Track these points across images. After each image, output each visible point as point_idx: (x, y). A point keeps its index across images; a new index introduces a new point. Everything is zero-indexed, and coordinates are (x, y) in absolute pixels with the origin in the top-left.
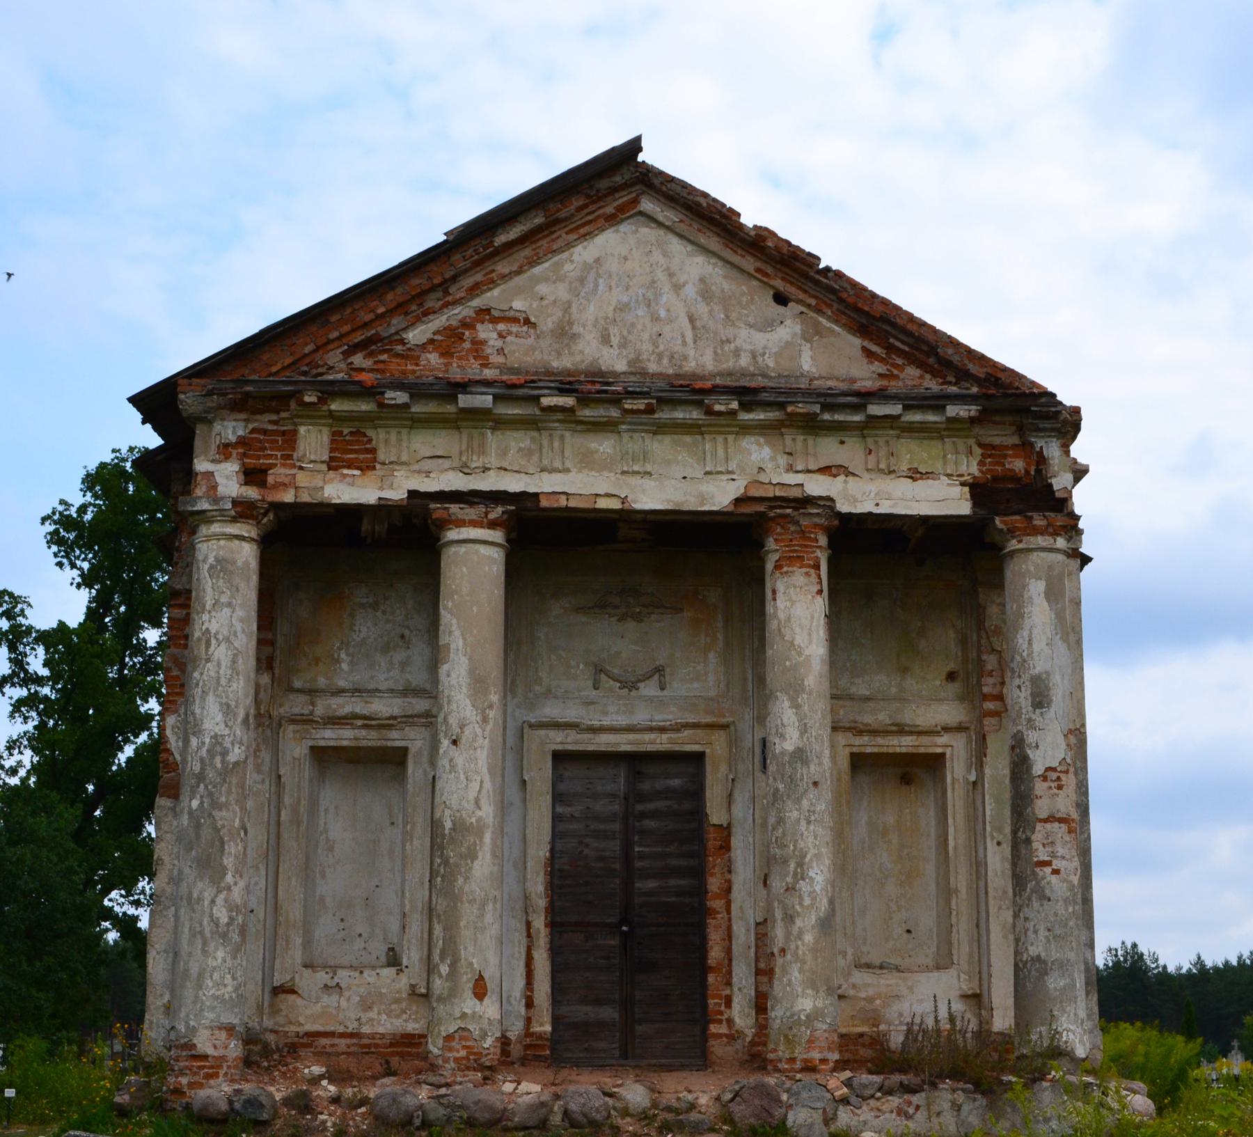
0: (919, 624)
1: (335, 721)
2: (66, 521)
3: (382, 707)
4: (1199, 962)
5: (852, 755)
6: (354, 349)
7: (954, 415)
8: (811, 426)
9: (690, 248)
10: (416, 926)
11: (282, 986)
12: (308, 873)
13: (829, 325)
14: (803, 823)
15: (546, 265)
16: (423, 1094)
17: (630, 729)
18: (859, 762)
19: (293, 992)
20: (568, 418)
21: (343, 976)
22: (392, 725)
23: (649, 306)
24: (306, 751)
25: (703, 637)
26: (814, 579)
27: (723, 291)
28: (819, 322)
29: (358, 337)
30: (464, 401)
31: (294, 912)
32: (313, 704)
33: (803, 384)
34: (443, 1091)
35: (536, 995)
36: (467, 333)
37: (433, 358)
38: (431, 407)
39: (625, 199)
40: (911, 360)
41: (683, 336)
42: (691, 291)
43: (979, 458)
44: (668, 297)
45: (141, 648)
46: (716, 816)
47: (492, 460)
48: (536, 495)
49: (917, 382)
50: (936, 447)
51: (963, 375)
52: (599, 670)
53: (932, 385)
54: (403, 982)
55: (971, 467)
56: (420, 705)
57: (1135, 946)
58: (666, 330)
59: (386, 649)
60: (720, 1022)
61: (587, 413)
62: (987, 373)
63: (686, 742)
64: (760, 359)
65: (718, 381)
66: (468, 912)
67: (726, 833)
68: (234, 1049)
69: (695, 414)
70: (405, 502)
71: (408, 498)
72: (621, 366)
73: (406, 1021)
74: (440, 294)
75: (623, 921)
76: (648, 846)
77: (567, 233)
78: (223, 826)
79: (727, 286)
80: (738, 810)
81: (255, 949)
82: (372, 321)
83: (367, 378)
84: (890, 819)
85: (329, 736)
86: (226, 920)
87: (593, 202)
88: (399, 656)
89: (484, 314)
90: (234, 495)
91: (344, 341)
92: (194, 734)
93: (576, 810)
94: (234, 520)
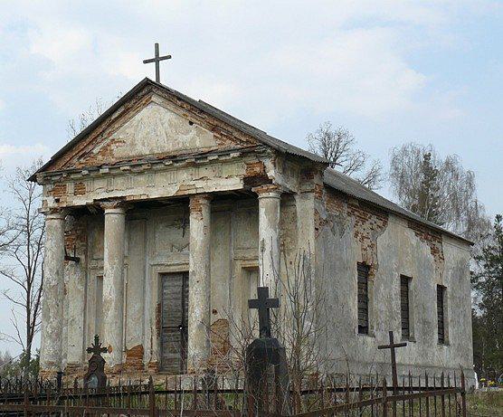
17: (178, 265)
29: (81, 154)
30: (102, 171)
37: (100, 157)
42: (166, 125)
55: (243, 172)
61: (222, 159)
72: (148, 153)
94: (51, 214)
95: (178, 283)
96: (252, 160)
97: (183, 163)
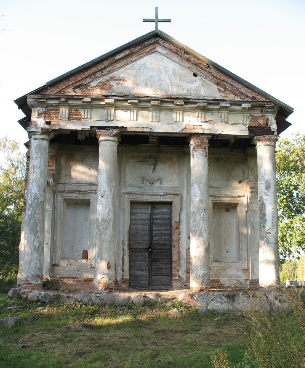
0: (232, 168)
1: (71, 192)
5: (213, 203)
7: (244, 107)
9: (170, 61)
11: (55, 264)
13: (209, 82)
14: (201, 221)
15: (130, 65)
19: (58, 266)
20: (135, 106)
22: (86, 193)
23: (159, 76)
24: (62, 200)
25: (172, 170)
26: (204, 152)
27: (179, 73)
28: (206, 82)
29: (77, 84)
32: (65, 187)
33: (202, 98)
34: (98, 295)
35: (125, 268)
36: (108, 83)
39: (152, 47)
41: (168, 84)
42: (170, 73)
43: (251, 119)
48: (126, 128)
49: (233, 98)
52: (143, 179)
58: (163, 83)
60: (176, 276)
62: (253, 96)
63: (168, 199)
64: (190, 91)
65: (178, 97)
67: (178, 224)
70: (89, 129)
71: (91, 128)
73: (89, 274)
74: (100, 72)
75: (150, 248)
76: (156, 227)
77: (136, 56)
78: (37, 219)
82: (81, 80)
85: (68, 196)
86: (38, 246)
87: (143, 48)
89: (112, 78)
90: (42, 127)
91: (74, 85)
92: (30, 193)
95: (146, 211)
97: (194, 106)
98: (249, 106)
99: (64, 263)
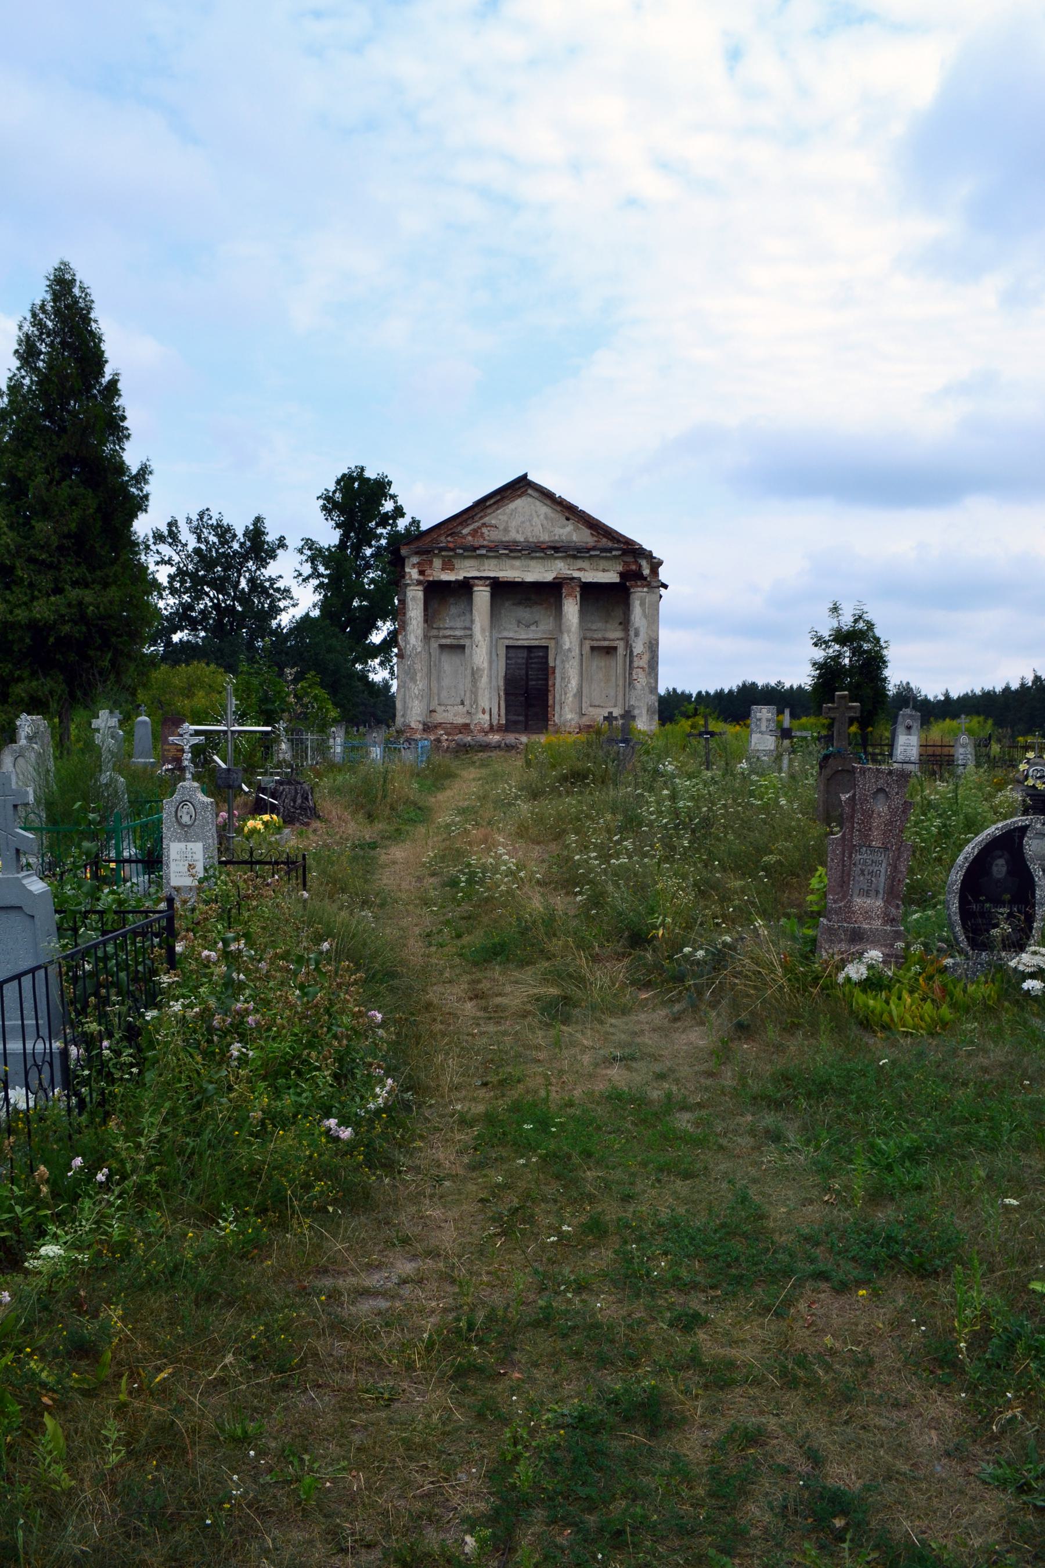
2: (328, 499)
3: (458, 633)
4: (947, 695)
6: (448, 536)
8: (575, 557)
10: (468, 695)
12: (439, 679)
16: (469, 738)
18: (593, 648)
21: (449, 708)
30: (478, 552)
31: (435, 690)
37: (470, 538)
38: (469, 554)
40: (604, 536)
42: (542, 517)
44: (535, 519)
45: (364, 558)
46: (551, 664)
47: (486, 568)
50: (610, 562)
51: (619, 541)
53: (610, 544)
54: (465, 709)
55: (620, 568)
56: (468, 632)
57: (908, 683)
59: (459, 616)
61: (512, 555)
63: (543, 643)
66: (480, 692)
68: (421, 727)
69: (542, 555)
72: (522, 540)
79: (553, 515)
80: (558, 662)
81: (425, 701)
83: (451, 545)
84: (603, 664)
85: (444, 641)
88: (463, 618)
89: (484, 525)
93: (513, 662)
96: (629, 559)
98: (620, 553)
99: (440, 709)
